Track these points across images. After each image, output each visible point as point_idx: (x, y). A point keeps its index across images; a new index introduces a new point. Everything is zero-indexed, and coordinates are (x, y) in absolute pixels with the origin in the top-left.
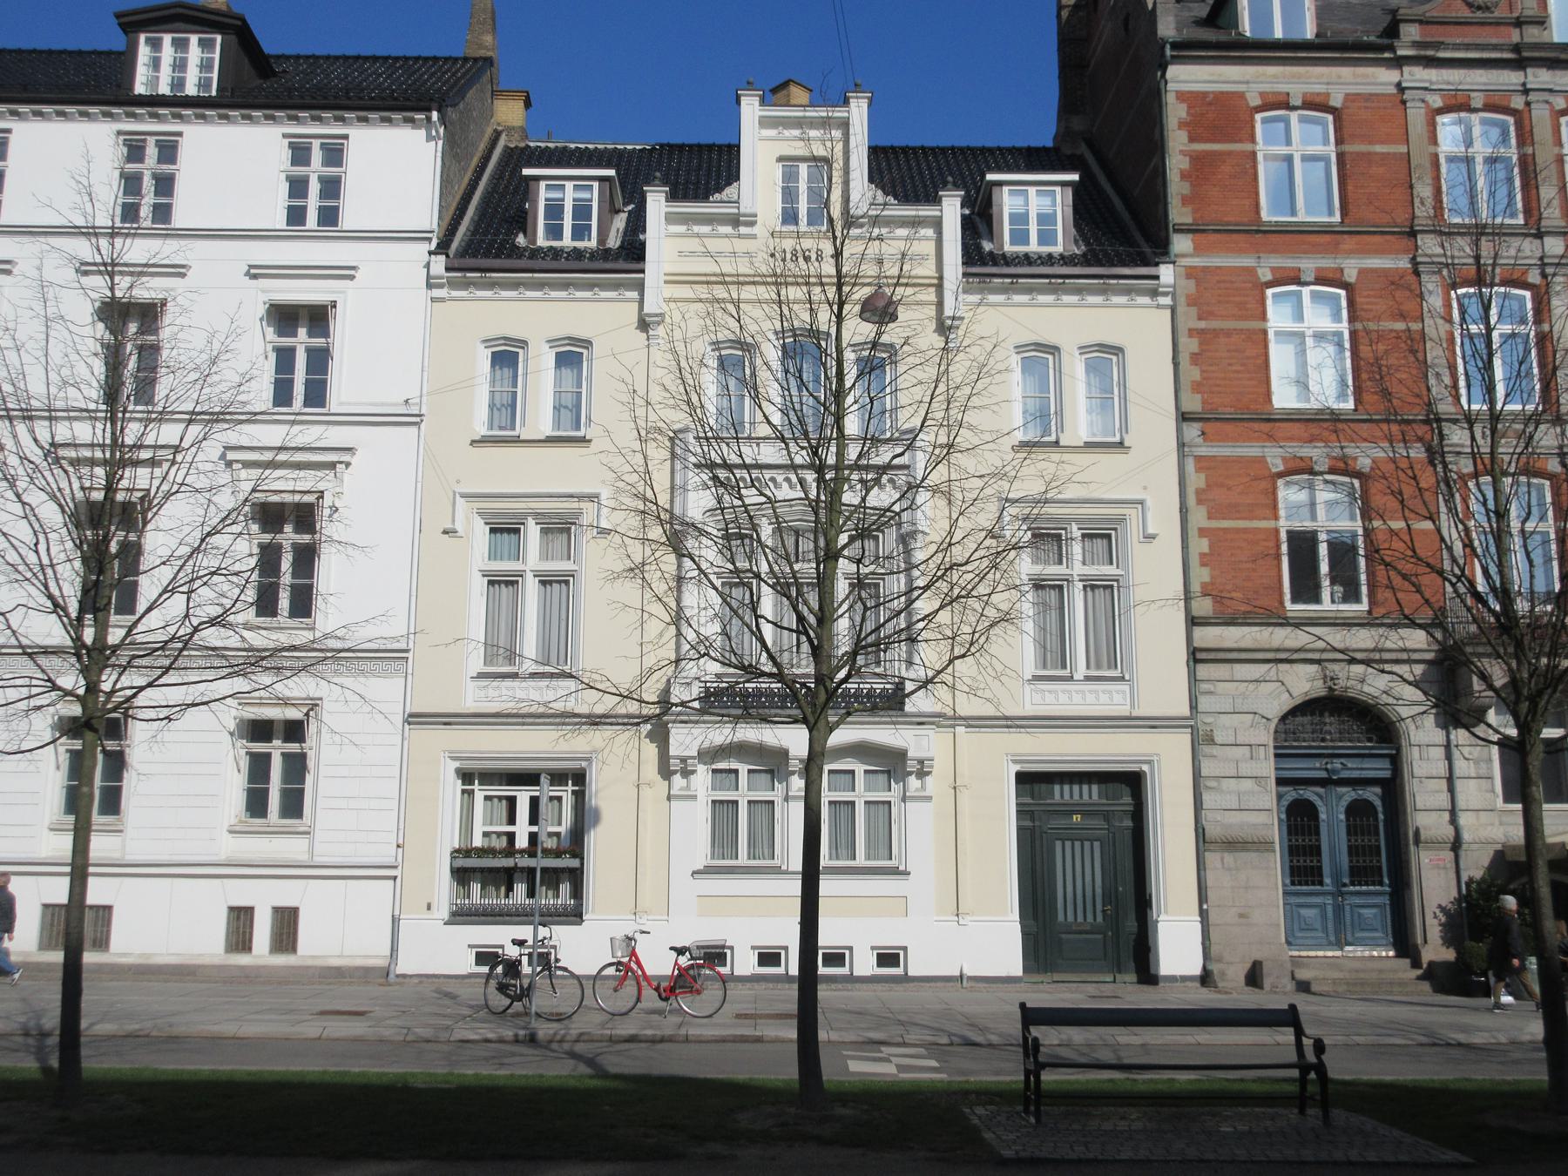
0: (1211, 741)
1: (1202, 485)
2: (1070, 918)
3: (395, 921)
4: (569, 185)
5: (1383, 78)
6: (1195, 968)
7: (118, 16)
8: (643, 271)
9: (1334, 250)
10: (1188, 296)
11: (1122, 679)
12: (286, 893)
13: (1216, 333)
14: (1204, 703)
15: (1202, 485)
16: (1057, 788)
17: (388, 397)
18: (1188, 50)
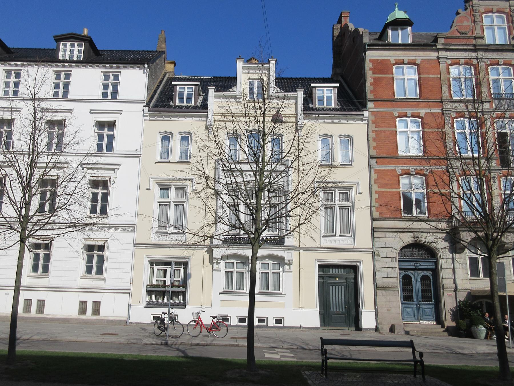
0: (379, 256)
1: (376, 177)
2: (335, 310)
3: (129, 306)
4: (186, 87)
5: (432, 55)
6: (374, 327)
9: (417, 107)
12: (97, 297)
13: (381, 132)
14: (376, 244)
15: (376, 177)
16: (331, 270)
17: (131, 149)
18: (372, 46)
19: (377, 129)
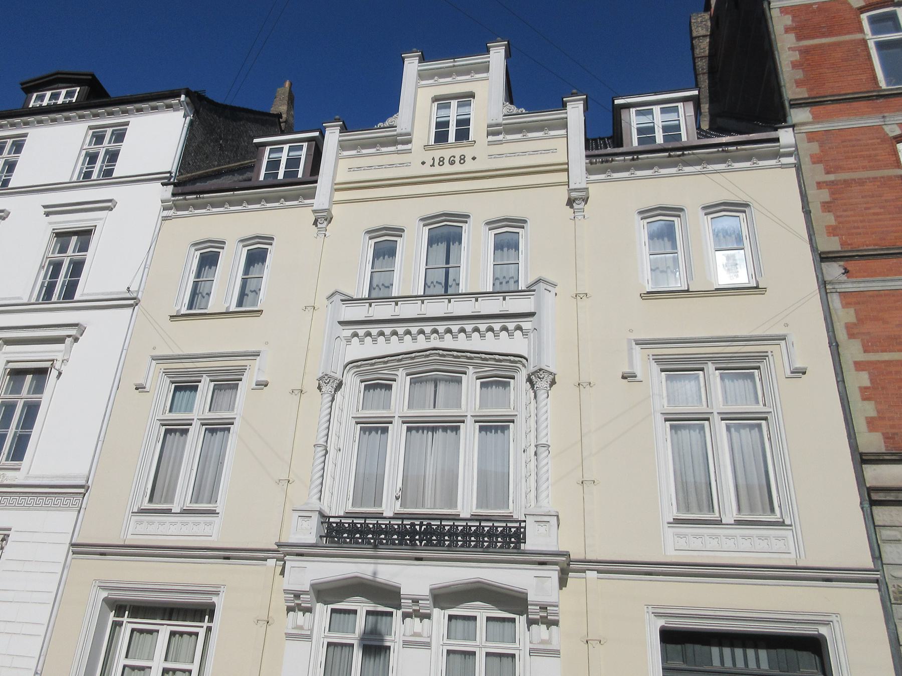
4: (286, 147)
7: (22, 84)
8: (316, 182)
10: (812, 156)
11: (782, 524)
14: (890, 553)
16: (715, 650)
17: (117, 287)
19: (831, 177)
